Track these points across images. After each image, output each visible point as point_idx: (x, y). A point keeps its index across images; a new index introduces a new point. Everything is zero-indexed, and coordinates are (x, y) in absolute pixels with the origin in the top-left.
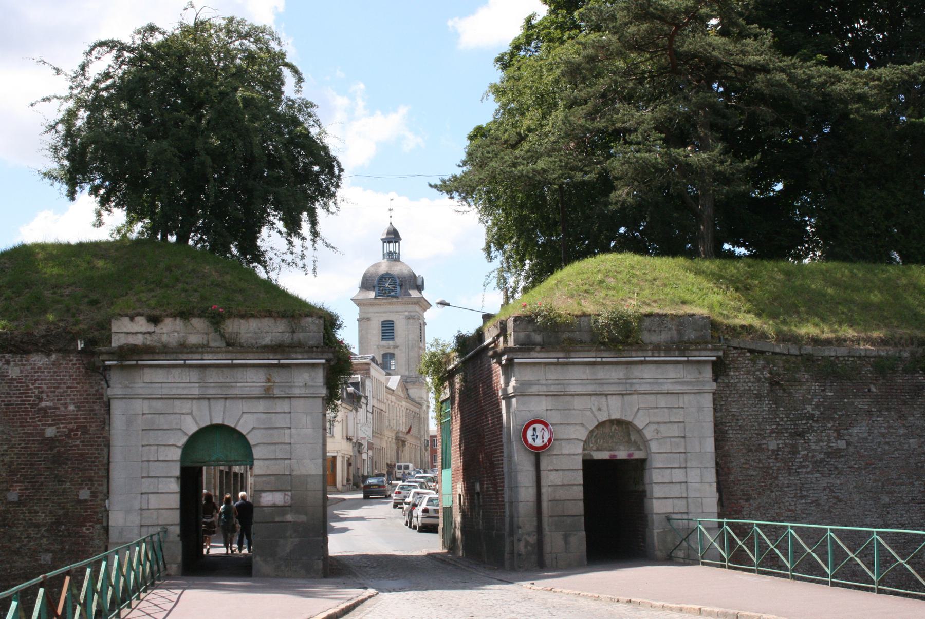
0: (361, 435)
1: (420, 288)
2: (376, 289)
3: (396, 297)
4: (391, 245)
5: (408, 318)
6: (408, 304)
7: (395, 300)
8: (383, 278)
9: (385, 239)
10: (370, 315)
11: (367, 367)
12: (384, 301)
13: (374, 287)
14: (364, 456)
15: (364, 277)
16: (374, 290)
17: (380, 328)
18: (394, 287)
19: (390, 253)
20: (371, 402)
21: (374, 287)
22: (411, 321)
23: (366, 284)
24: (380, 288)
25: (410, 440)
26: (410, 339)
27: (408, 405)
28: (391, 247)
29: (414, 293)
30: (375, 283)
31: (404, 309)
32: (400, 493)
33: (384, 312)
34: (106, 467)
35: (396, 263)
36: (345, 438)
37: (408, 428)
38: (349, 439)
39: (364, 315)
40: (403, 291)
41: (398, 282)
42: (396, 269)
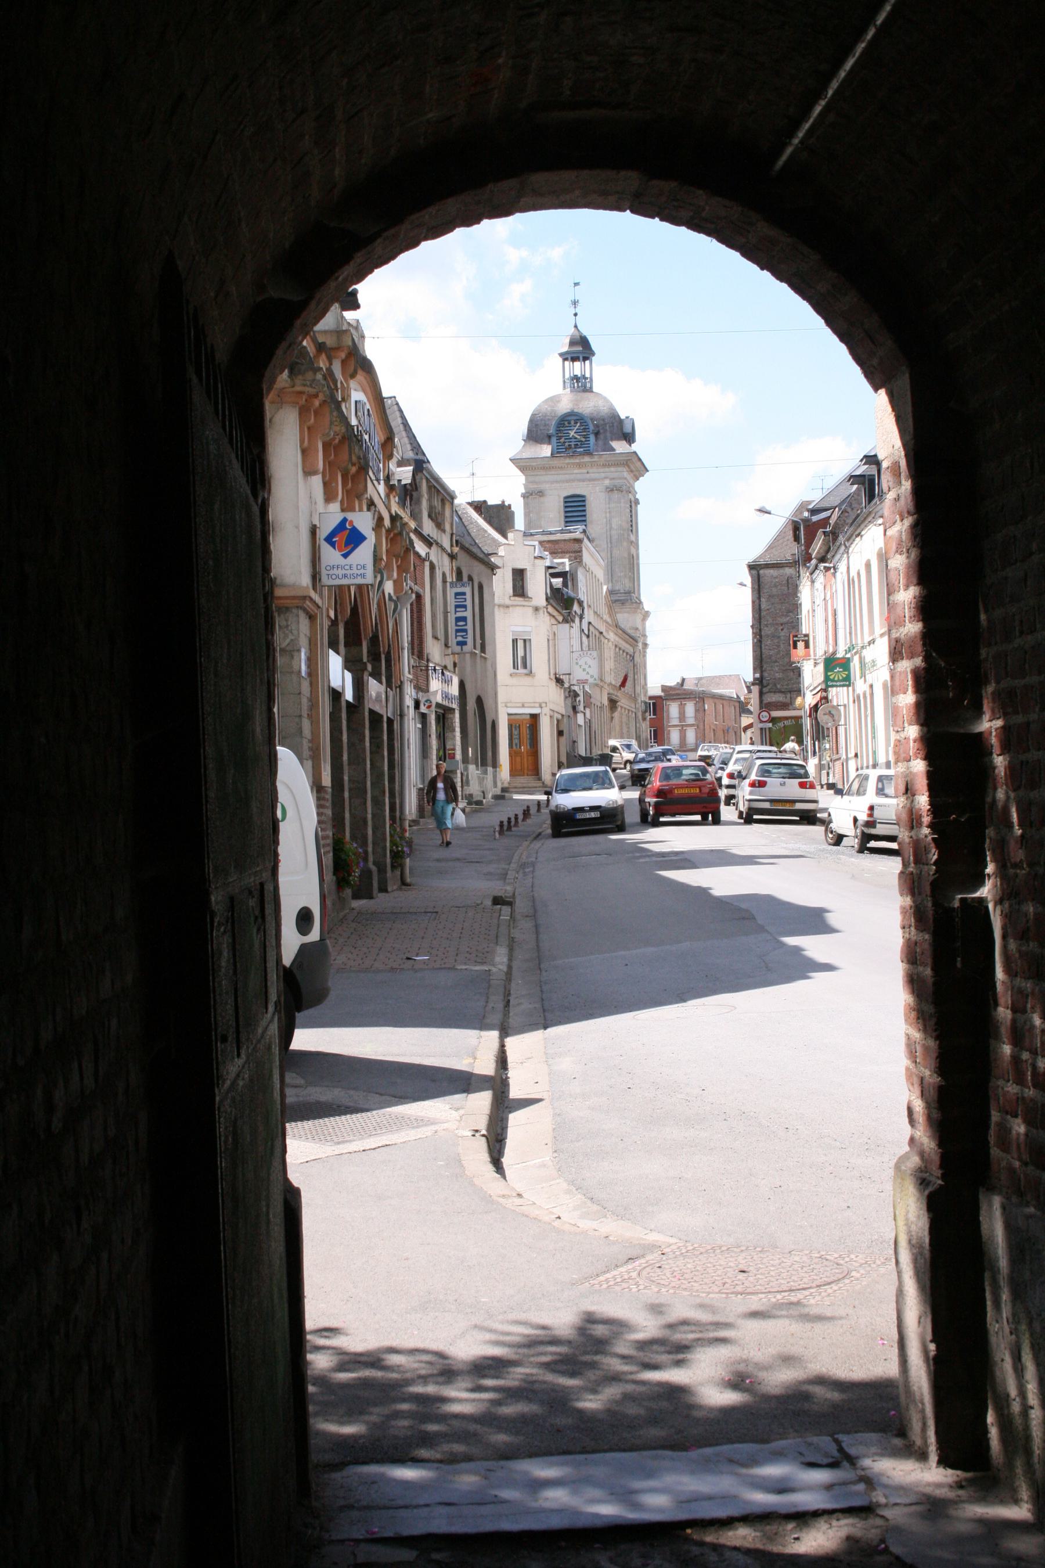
0: (579, 674)
1: (629, 437)
2: (554, 440)
3: (588, 453)
4: (577, 364)
5: (610, 490)
6: (609, 466)
7: (587, 459)
8: (566, 421)
9: (567, 353)
10: (543, 487)
11: (576, 546)
12: (568, 461)
13: (549, 437)
14: (580, 719)
15: (531, 421)
16: (549, 443)
17: (562, 509)
18: (585, 437)
19: (576, 378)
20: (589, 616)
21: (549, 437)
22: (616, 495)
23: (536, 433)
24: (560, 438)
25: (623, 702)
26: (614, 526)
27: (617, 639)
28: (577, 368)
29: (620, 447)
30: (552, 431)
31: (603, 475)
32: (762, 784)
33: (567, 481)
34: (544, 996)
35: (587, 395)
36: (553, 677)
37: (620, 680)
38: (559, 681)
39: (533, 487)
40: (600, 443)
41: (591, 427)
42: (587, 406)
